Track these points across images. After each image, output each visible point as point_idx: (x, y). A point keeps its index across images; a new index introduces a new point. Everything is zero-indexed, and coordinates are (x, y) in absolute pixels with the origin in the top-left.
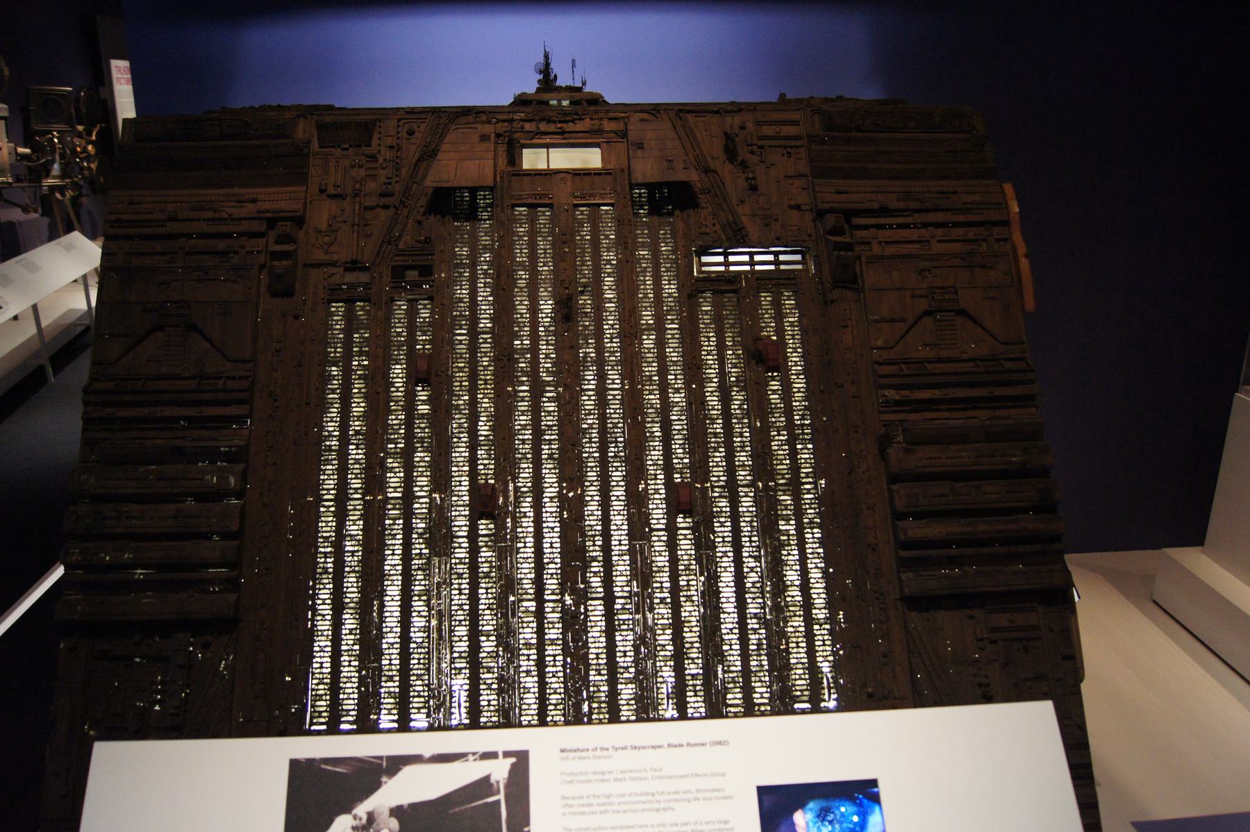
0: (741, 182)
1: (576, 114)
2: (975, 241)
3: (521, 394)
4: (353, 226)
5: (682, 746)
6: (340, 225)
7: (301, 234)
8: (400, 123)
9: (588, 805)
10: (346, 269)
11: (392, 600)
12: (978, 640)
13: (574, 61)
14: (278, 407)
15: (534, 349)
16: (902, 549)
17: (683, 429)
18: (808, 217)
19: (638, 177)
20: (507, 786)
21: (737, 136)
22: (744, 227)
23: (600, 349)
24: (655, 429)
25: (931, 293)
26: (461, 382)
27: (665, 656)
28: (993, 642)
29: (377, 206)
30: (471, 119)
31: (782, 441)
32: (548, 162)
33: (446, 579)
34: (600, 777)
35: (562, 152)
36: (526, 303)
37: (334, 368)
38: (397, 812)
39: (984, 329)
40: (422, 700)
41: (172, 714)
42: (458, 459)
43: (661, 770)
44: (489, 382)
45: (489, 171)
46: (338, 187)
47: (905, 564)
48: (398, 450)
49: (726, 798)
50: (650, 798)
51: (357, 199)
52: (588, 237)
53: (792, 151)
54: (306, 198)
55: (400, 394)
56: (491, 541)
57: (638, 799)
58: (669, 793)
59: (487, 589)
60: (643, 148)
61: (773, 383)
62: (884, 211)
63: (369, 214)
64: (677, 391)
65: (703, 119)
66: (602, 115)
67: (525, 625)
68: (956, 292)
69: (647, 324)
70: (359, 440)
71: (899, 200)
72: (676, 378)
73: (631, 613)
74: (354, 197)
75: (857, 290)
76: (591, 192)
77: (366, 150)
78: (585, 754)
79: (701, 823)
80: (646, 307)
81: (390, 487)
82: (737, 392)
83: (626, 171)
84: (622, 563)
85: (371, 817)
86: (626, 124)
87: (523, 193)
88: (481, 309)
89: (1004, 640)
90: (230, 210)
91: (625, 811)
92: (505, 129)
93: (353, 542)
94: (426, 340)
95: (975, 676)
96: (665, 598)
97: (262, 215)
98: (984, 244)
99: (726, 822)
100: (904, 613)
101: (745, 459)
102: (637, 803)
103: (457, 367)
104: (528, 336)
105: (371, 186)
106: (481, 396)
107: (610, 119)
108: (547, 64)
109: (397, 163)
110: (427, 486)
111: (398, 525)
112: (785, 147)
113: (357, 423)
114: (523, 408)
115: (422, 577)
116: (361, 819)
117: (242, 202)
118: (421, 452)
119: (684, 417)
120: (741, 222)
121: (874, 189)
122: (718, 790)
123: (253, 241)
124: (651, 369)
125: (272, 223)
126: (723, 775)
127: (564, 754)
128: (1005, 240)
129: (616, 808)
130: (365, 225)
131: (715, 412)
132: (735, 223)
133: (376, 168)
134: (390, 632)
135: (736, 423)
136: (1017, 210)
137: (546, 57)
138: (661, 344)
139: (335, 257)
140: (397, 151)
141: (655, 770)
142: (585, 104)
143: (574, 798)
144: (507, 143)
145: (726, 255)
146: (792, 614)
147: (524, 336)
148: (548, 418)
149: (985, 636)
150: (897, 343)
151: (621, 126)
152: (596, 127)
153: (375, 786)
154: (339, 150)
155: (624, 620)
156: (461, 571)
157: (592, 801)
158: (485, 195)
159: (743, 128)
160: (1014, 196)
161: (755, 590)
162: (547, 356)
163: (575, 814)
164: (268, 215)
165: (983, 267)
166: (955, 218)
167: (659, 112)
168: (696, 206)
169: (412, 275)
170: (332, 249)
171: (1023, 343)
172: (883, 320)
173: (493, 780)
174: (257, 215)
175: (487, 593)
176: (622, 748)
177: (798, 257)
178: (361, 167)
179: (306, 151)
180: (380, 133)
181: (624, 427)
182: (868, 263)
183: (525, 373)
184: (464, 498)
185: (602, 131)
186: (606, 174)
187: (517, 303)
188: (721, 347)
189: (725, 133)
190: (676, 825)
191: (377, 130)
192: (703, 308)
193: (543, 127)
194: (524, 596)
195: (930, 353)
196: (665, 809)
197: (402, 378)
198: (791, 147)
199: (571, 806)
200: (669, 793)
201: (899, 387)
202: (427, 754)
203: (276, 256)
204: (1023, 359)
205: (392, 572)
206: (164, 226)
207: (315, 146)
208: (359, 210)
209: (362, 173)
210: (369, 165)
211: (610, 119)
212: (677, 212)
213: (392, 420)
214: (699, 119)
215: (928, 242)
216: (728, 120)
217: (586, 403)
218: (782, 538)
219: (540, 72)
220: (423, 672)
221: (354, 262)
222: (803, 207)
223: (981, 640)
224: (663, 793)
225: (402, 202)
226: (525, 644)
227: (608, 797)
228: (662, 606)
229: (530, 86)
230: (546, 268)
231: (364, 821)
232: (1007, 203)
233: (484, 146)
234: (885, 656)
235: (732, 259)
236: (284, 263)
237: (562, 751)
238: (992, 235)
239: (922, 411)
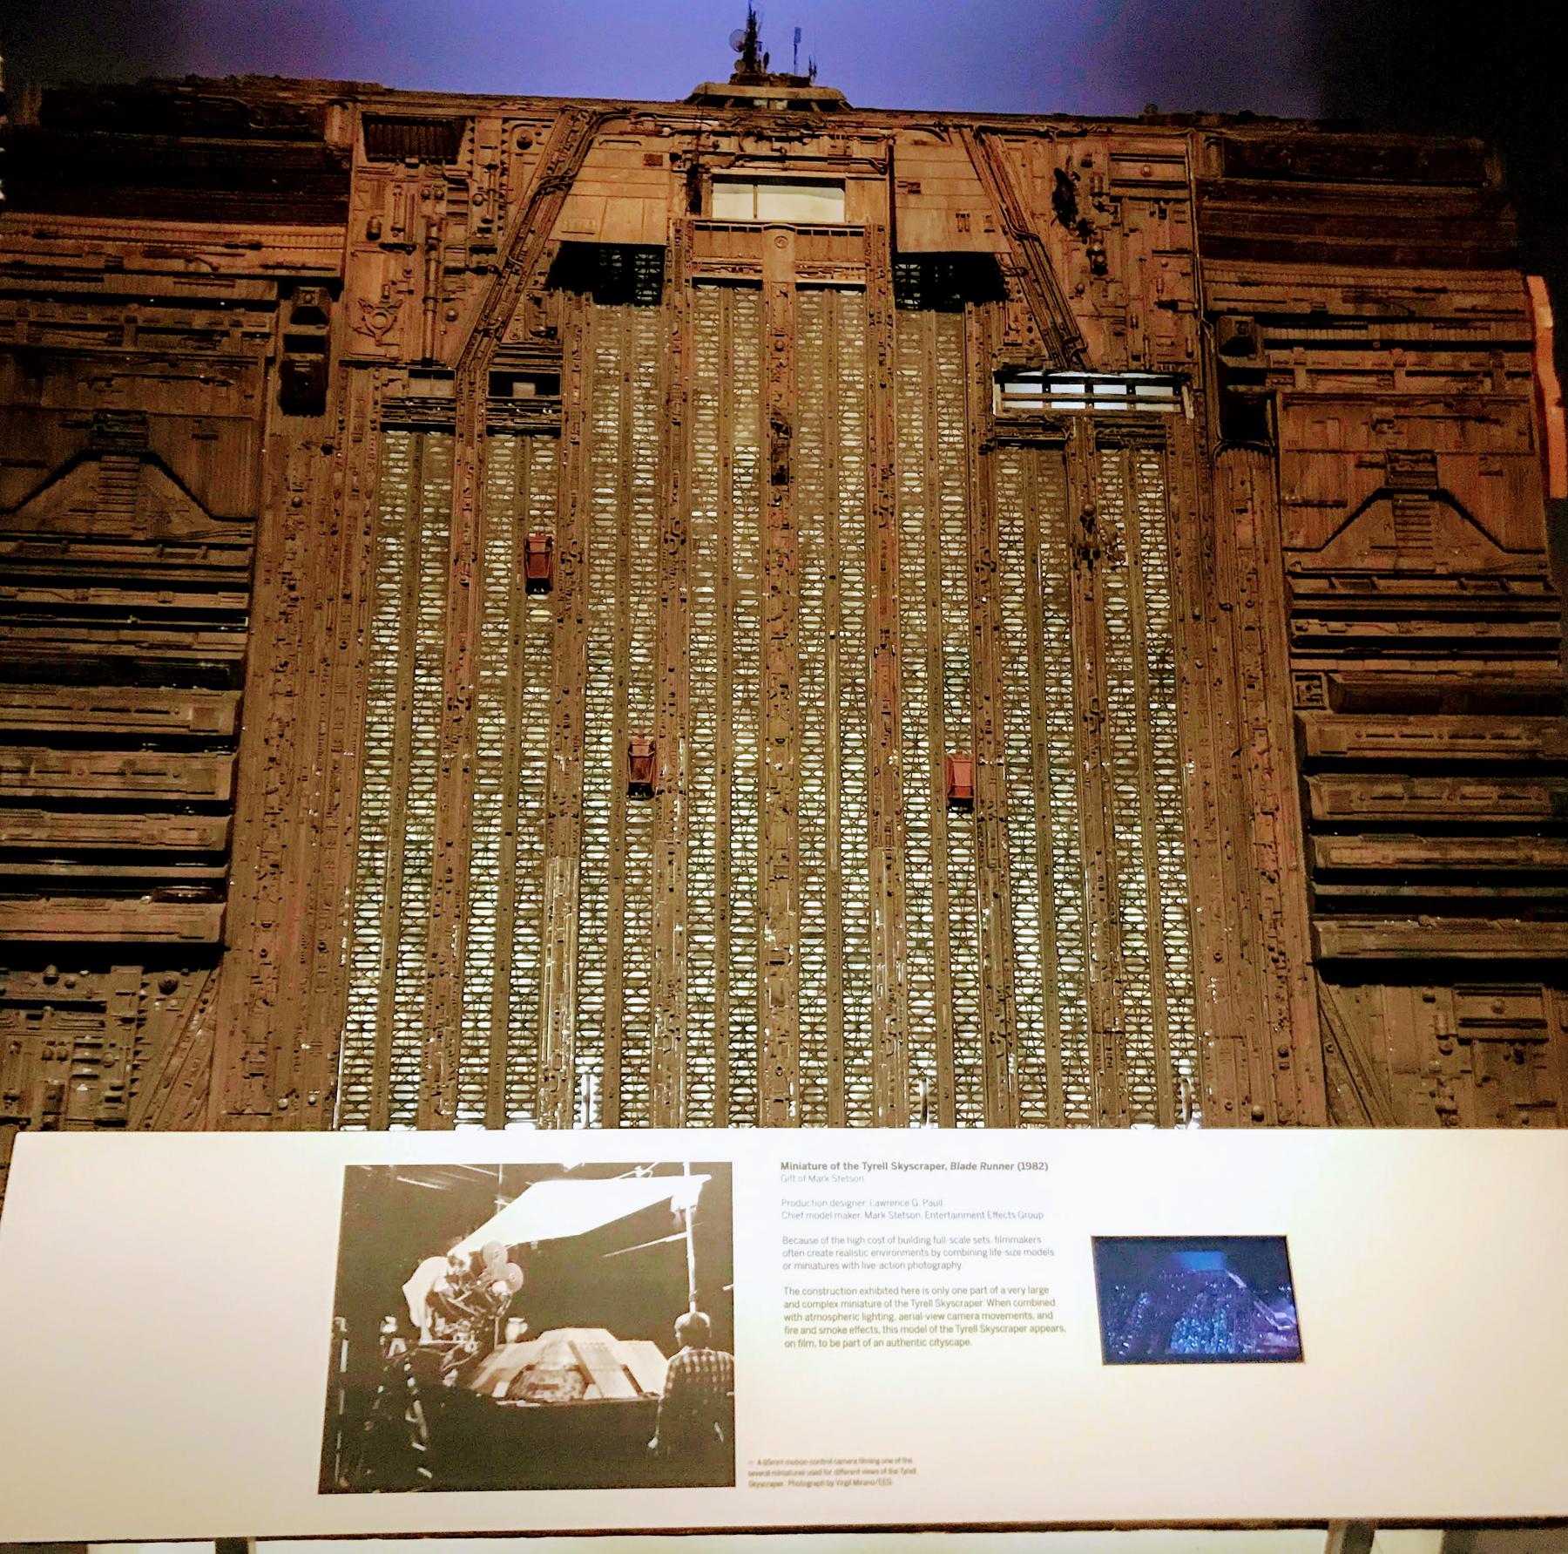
0: (1080, 258)
1: (807, 127)
2: (1472, 375)
3: (701, 600)
4: (425, 300)
5: (974, 1167)
6: (401, 297)
7: (336, 309)
8: (506, 126)
9: (824, 1254)
10: (414, 374)
11: (483, 924)
12: (1440, 1037)
13: (798, 31)
14: (296, 599)
15: (724, 526)
16: (1319, 882)
17: (964, 669)
18: (1190, 326)
19: (907, 244)
20: (695, 1220)
21: (1078, 178)
22: (1080, 336)
23: (831, 533)
24: (917, 667)
25: (1391, 461)
26: (603, 574)
27: (923, 1033)
28: (1465, 1042)
29: (467, 268)
30: (626, 125)
31: (1124, 695)
32: (756, 209)
33: (571, 893)
34: (844, 1210)
35: (812, 194)
36: (713, 448)
37: (390, 540)
38: (520, 1254)
39: (1477, 524)
40: (526, 1088)
41: (109, 1100)
42: (597, 700)
43: (940, 1203)
44: (649, 577)
45: (659, 218)
46: (400, 230)
47: (1321, 907)
48: (497, 681)
49: (1044, 1253)
50: (923, 1246)
51: (433, 254)
52: (819, 342)
53: (1170, 208)
54: (345, 248)
55: (501, 589)
56: (647, 835)
57: (904, 1247)
58: (953, 1241)
59: (638, 911)
60: (918, 192)
61: (1115, 600)
62: (1320, 318)
63: (451, 283)
64: (957, 605)
65: (1021, 145)
66: (850, 131)
67: (698, 973)
68: (1433, 461)
69: (911, 494)
70: (432, 660)
71: (1345, 300)
72: (955, 585)
73: (869, 962)
74: (428, 252)
75: (1264, 451)
76: (827, 264)
77: (447, 168)
78: (820, 1173)
79: (1003, 1291)
80: (911, 465)
81: (482, 740)
82: (1055, 611)
83: (888, 229)
84: (856, 879)
85: (479, 1263)
86: (891, 149)
87: (714, 260)
88: (639, 455)
89: (1481, 1040)
90: (215, 260)
91: (883, 1266)
92: (686, 147)
93: (419, 828)
94: (546, 501)
95: (1433, 1095)
96: (925, 940)
97: (270, 272)
98: (1488, 382)
99: (1043, 1291)
100: (1317, 986)
101: (1062, 722)
102: (903, 1253)
103: (598, 549)
104: (715, 504)
105: (456, 233)
106: (636, 599)
107: (863, 138)
108: (752, 35)
109: (502, 196)
110: (544, 741)
111: (496, 801)
112: (1157, 200)
113: (428, 633)
114: (703, 623)
115: (531, 889)
116: (461, 1264)
117: (237, 247)
118: (535, 686)
119: (965, 650)
120: (1077, 328)
121: (1298, 280)
122: (1031, 1240)
123: (255, 316)
124: (914, 568)
125: (288, 286)
126: (1040, 1216)
127: (788, 1172)
128: (1526, 375)
129: (869, 1260)
130: (447, 300)
131: (1017, 644)
132: (1066, 328)
133: (466, 202)
134: (476, 976)
135: (1050, 664)
136: (1549, 323)
137: (752, 22)
138: (933, 528)
139: (394, 352)
140: (502, 174)
141: (932, 1204)
142: (816, 108)
143: (802, 1241)
144: (687, 172)
145: (1046, 382)
146: (1131, 977)
147: (707, 503)
148: (744, 641)
149: (1453, 1032)
150: (1327, 542)
151: (879, 152)
152: (839, 152)
153: (484, 1214)
154: (402, 166)
155: (858, 972)
156: (596, 881)
157: (830, 1247)
158: (647, 260)
159: (1087, 164)
160: (1546, 298)
161: (1073, 935)
162: (745, 539)
163: (804, 1266)
164: (283, 272)
165: (1482, 419)
166: (1437, 335)
167: (946, 129)
168: (1002, 296)
169: (524, 390)
170: (388, 338)
171: (1542, 551)
172: (1307, 503)
173: (674, 1208)
174: (259, 271)
175: (639, 919)
176: (879, 1167)
177: (1167, 391)
178: (439, 198)
179: (345, 165)
180: (472, 141)
181: (866, 662)
182: (1286, 407)
183: (708, 566)
184: (605, 764)
185: (850, 158)
186: (853, 234)
187: (698, 447)
188: (1031, 537)
189: (1057, 172)
190: (964, 1291)
191: (467, 135)
192: (1006, 471)
193: (750, 146)
194: (697, 927)
195: (1385, 562)
196: (945, 1266)
197: (505, 563)
198: (1167, 201)
199: (798, 1254)
200: (953, 1241)
201: (1324, 616)
202: (569, 1165)
203: (293, 343)
204: (1542, 578)
205: (482, 879)
206: (102, 280)
207: (360, 156)
208: (437, 273)
209: (443, 208)
210: (455, 196)
211: (863, 138)
212: (970, 306)
213: (487, 630)
214: (1013, 145)
215: (1391, 373)
216: (1063, 149)
217: (807, 618)
218: (1120, 853)
219: (740, 49)
220: (528, 1042)
221: (426, 362)
222: (1182, 306)
223: (1446, 1037)
224: (943, 1240)
225: (508, 264)
226: (696, 1004)
227: (857, 1242)
228: (919, 952)
229: (720, 71)
230: (748, 392)
231: (467, 1268)
232: (1532, 313)
233: (652, 174)
234: (1285, 1055)
235: (1056, 389)
236: (311, 357)
237: (785, 1166)
238: (1502, 366)
239: (1363, 657)
